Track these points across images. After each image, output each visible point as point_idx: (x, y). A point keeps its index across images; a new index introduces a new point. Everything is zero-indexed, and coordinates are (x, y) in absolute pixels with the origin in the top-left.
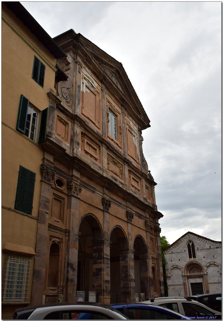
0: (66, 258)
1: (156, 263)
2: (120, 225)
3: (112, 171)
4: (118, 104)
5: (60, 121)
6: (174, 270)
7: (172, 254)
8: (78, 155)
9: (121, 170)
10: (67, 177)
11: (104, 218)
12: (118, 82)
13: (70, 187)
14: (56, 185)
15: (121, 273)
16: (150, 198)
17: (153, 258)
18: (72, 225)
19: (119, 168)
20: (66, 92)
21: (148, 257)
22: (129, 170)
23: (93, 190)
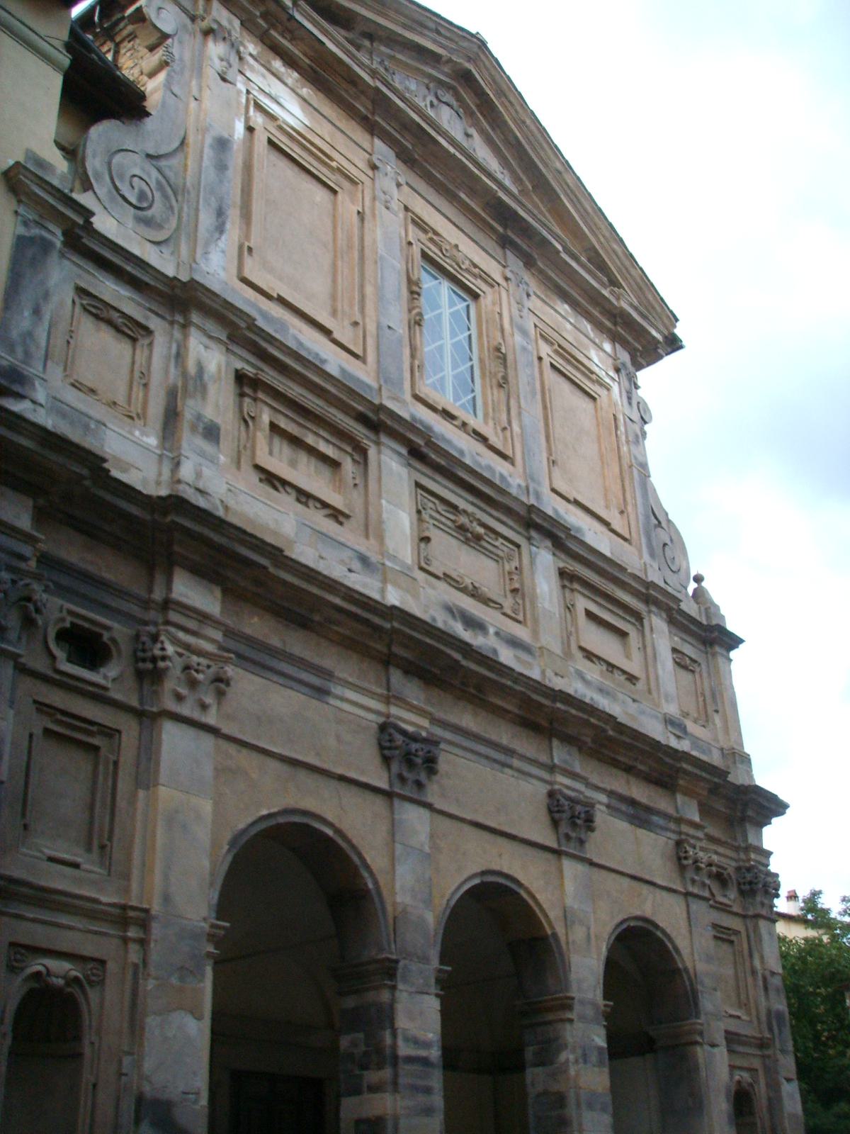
0: (124, 1071)
1: (756, 1063)
2: (505, 870)
3: (447, 578)
4: (479, 236)
5: (96, 317)
8: (209, 491)
9: (510, 573)
10: (135, 610)
12: (472, 131)
13: (149, 666)
14: (53, 657)
16: (707, 716)
17: (732, 1039)
19: (497, 559)
20: (137, 171)
21: (701, 1034)
22: (562, 574)
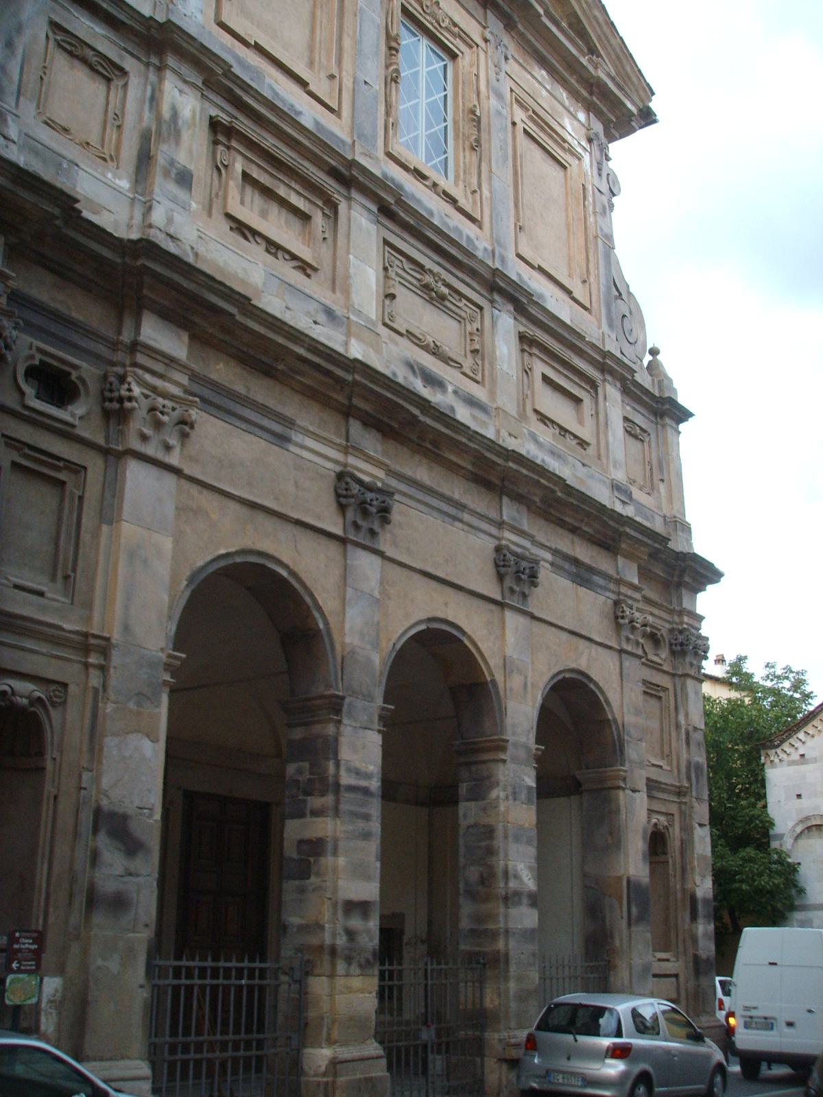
0: (84, 785)
1: (673, 809)
2: (450, 619)
3: (410, 335)
6: (809, 838)
7: (803, 764)
11: (345, 578)
13: (116, 405)
14: (22, 393)
15: (462, 860)
17: (652, 785)
18: (127, 608)
19: (460, 320)
21: (624, 779)
22: (522, 338)
23: (277, 428)
